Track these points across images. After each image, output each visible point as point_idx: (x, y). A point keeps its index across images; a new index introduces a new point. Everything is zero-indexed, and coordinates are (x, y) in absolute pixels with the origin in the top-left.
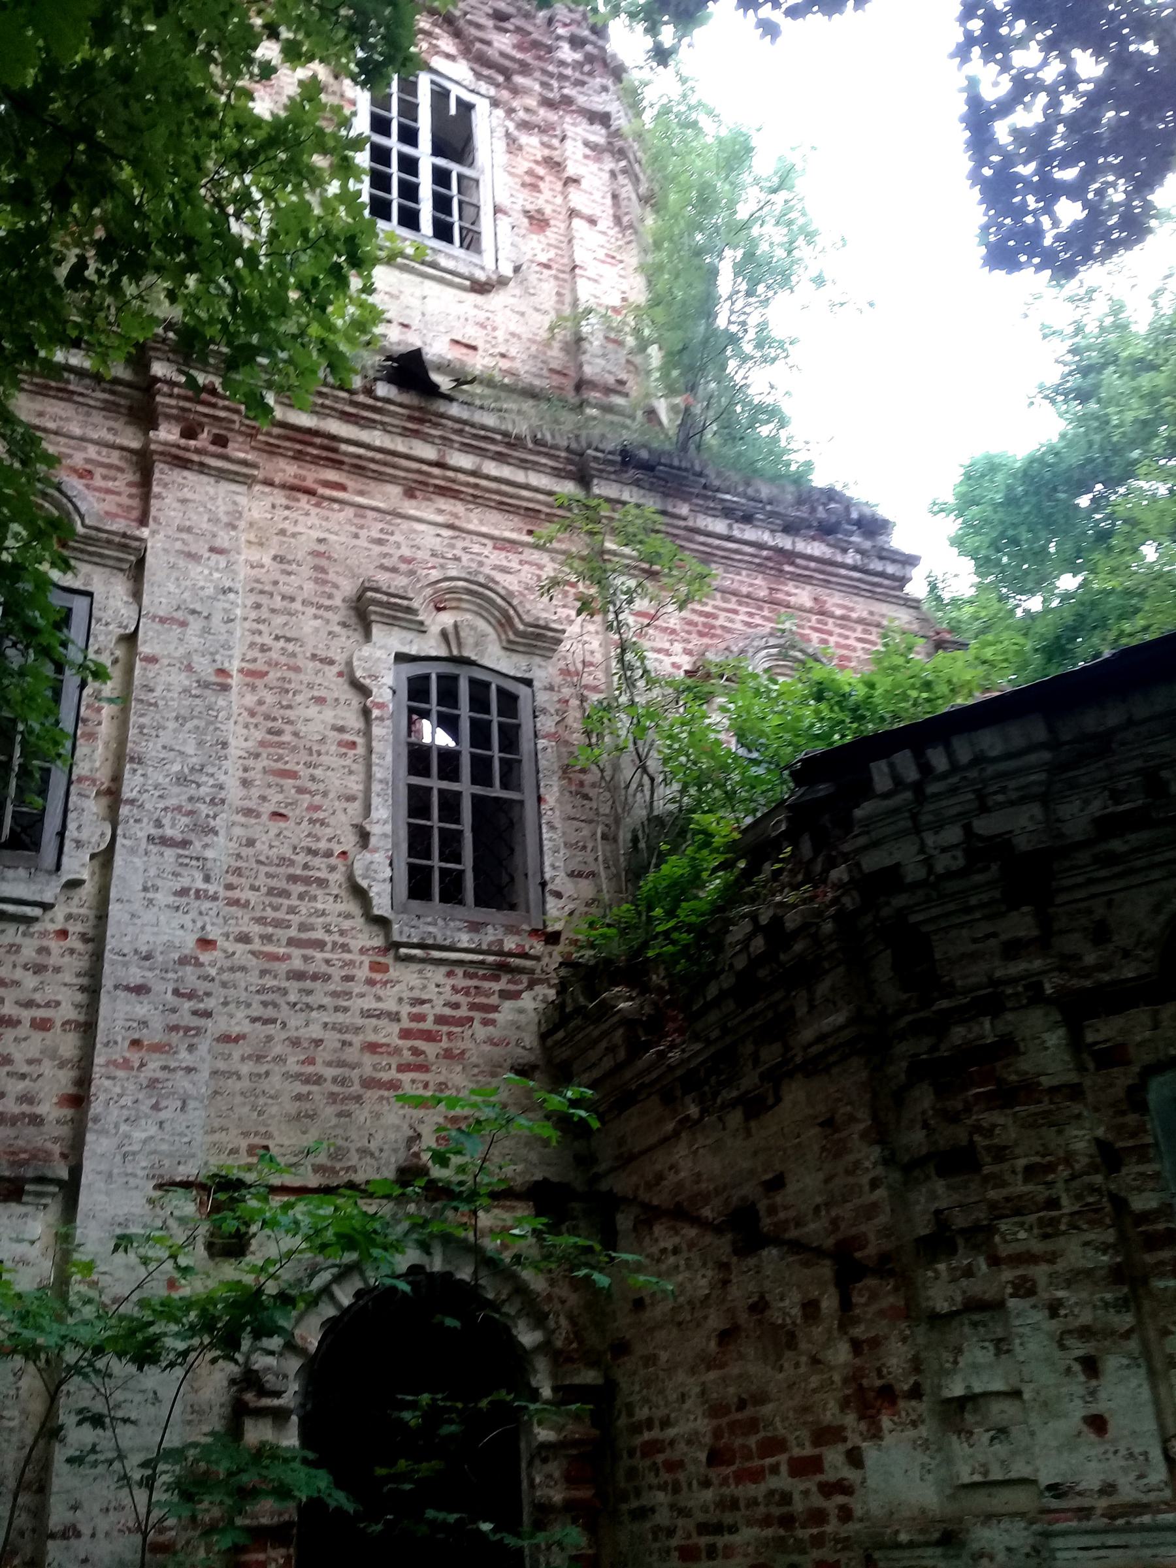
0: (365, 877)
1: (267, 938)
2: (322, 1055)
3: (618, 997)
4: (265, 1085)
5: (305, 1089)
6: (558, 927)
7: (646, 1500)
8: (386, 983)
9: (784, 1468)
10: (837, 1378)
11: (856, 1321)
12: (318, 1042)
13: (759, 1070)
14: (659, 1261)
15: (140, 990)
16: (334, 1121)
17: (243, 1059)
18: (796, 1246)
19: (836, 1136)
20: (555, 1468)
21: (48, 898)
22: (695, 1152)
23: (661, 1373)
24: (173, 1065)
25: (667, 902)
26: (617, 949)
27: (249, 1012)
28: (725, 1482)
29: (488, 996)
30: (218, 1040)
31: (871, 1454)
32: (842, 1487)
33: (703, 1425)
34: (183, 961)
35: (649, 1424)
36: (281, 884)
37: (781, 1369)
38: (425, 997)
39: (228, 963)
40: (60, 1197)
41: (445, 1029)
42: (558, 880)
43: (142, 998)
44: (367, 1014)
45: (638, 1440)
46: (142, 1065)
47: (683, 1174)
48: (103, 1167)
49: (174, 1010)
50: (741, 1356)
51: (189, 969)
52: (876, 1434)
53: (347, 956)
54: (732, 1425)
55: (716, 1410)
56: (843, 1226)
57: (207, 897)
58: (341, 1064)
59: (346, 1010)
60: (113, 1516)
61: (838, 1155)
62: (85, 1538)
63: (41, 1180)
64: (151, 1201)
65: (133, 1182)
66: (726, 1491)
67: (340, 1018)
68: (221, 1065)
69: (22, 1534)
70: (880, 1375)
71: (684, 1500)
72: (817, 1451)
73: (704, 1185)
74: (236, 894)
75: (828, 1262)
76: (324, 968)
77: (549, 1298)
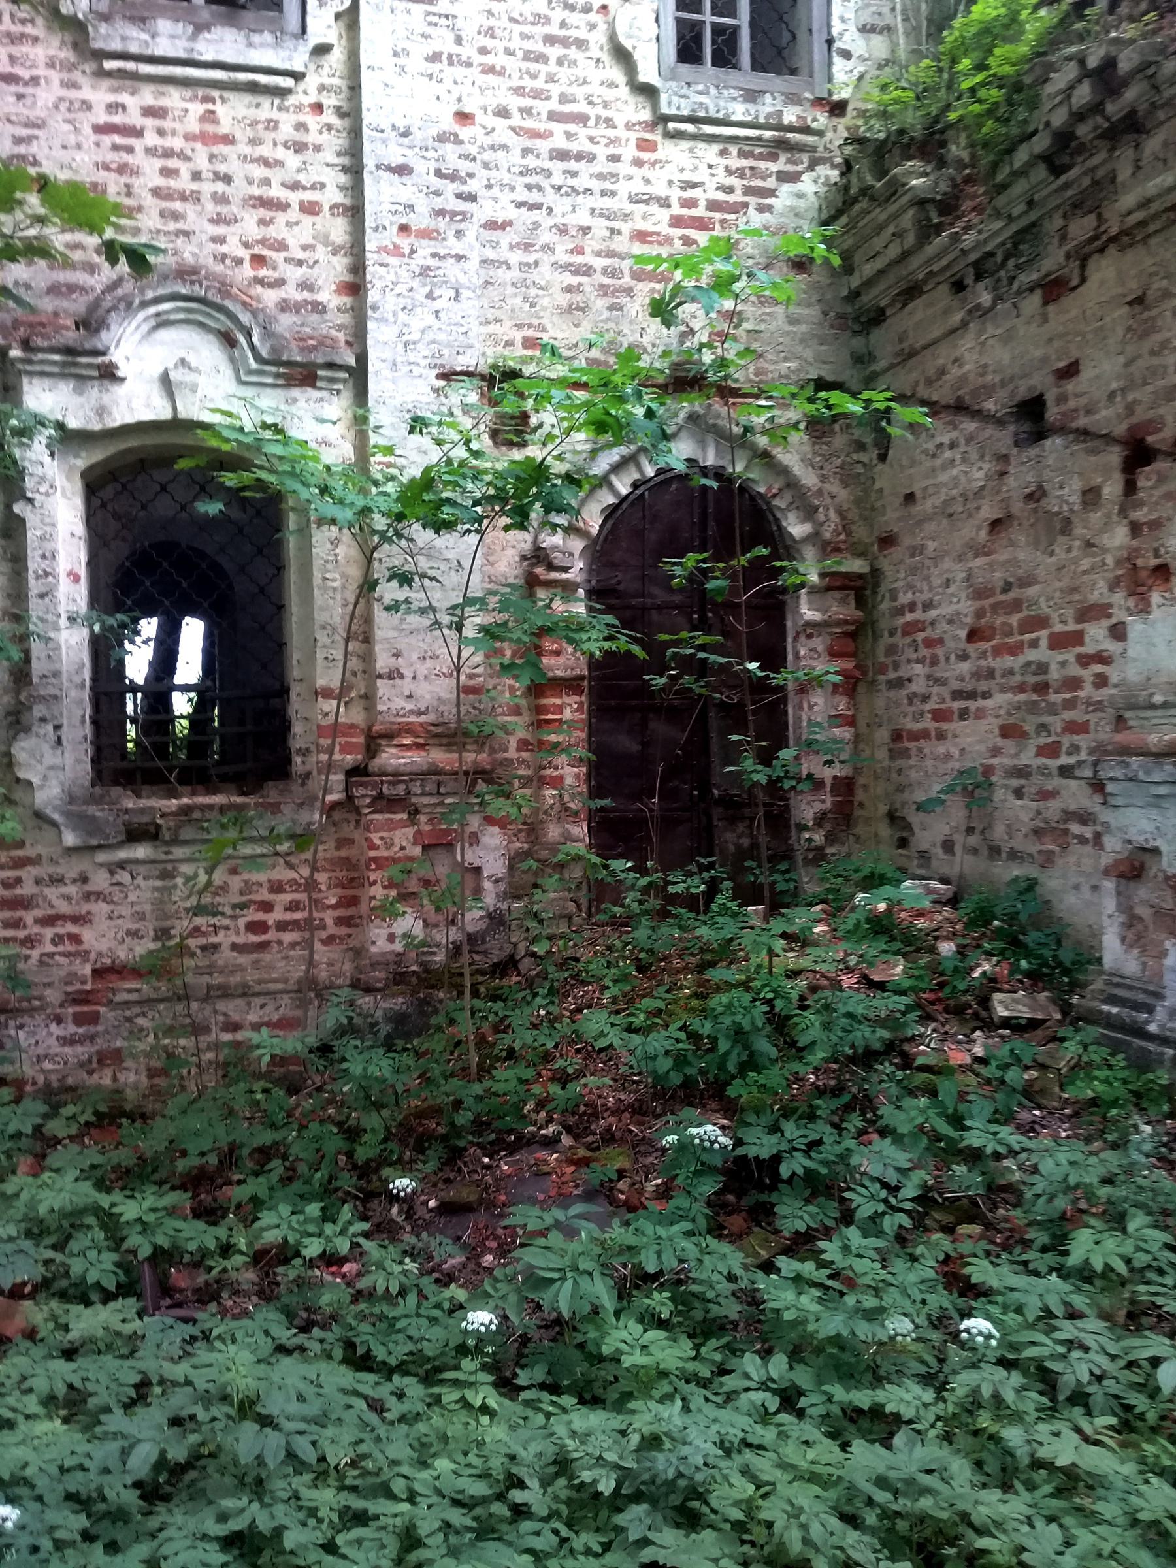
0: (630, 37)
1: (526, 112)
2: (591, 244)
3: (910, 173)
4: (534, 275)
5: (574, 280)
6: (845, 94)
7: (903, 673)
8: (654, 164)
9: (1044, 643)
10: (1110, 560)
11: (1139, 505)
12: (586, 230)
13: (1066, 248)
14: (934, 456)
15: (402, 170)
16: (606, 314)
17: (511, 247)
18: (1085, 434)
19: (1146, 314)
20: (819, 644)
21: (298, 67)
22: (983, 344)
23: (928, 562)
24: (442, 252)
25: (976, 55)
26: (914, 121)
27: (513, 196)
28: (983, 655)
29: (764, 178)
30: (484, 226)
31: (1136, 627)
32: (1102, 658)
33: (966, 607)
34: (442, 138)
35: (912, 607)
36: (538, 46)
37: (1052, 554)
38: (696, 179)
39: (488, 141)
40: (351, 383)
41: (718, 216)
42: (847, 36)
43: (405, 179)
44: (635, 199)
45: (900, 621)
46: (413, 252)
47: (967, 367)
48: (388, 355)
49: (438, 193)
50: (1012, 544)
51: (449, 147)
52: (1144, 609)
53: (611, 133)
54: (995, 607)
55: (980, 593)
56: (1139, 410)
57: (460, 63)
58: (611, 254)
59: (613, 194)
60: (429, 663)
61: (1145, 335)
62: (408, 680)
63: (330, 366)
64: (436, 391)
65: (417, 371)
66: (983, 663)
67: (607, 203)
68: (490, 254)
69: (355, 674)
70: (1157, 554)
71: (939, 672)
72: (1079, 627)
73: (989, 378)
74: (488, 60)
75: (1117, 449)
76: (588, 147)
77: (820, 492)
